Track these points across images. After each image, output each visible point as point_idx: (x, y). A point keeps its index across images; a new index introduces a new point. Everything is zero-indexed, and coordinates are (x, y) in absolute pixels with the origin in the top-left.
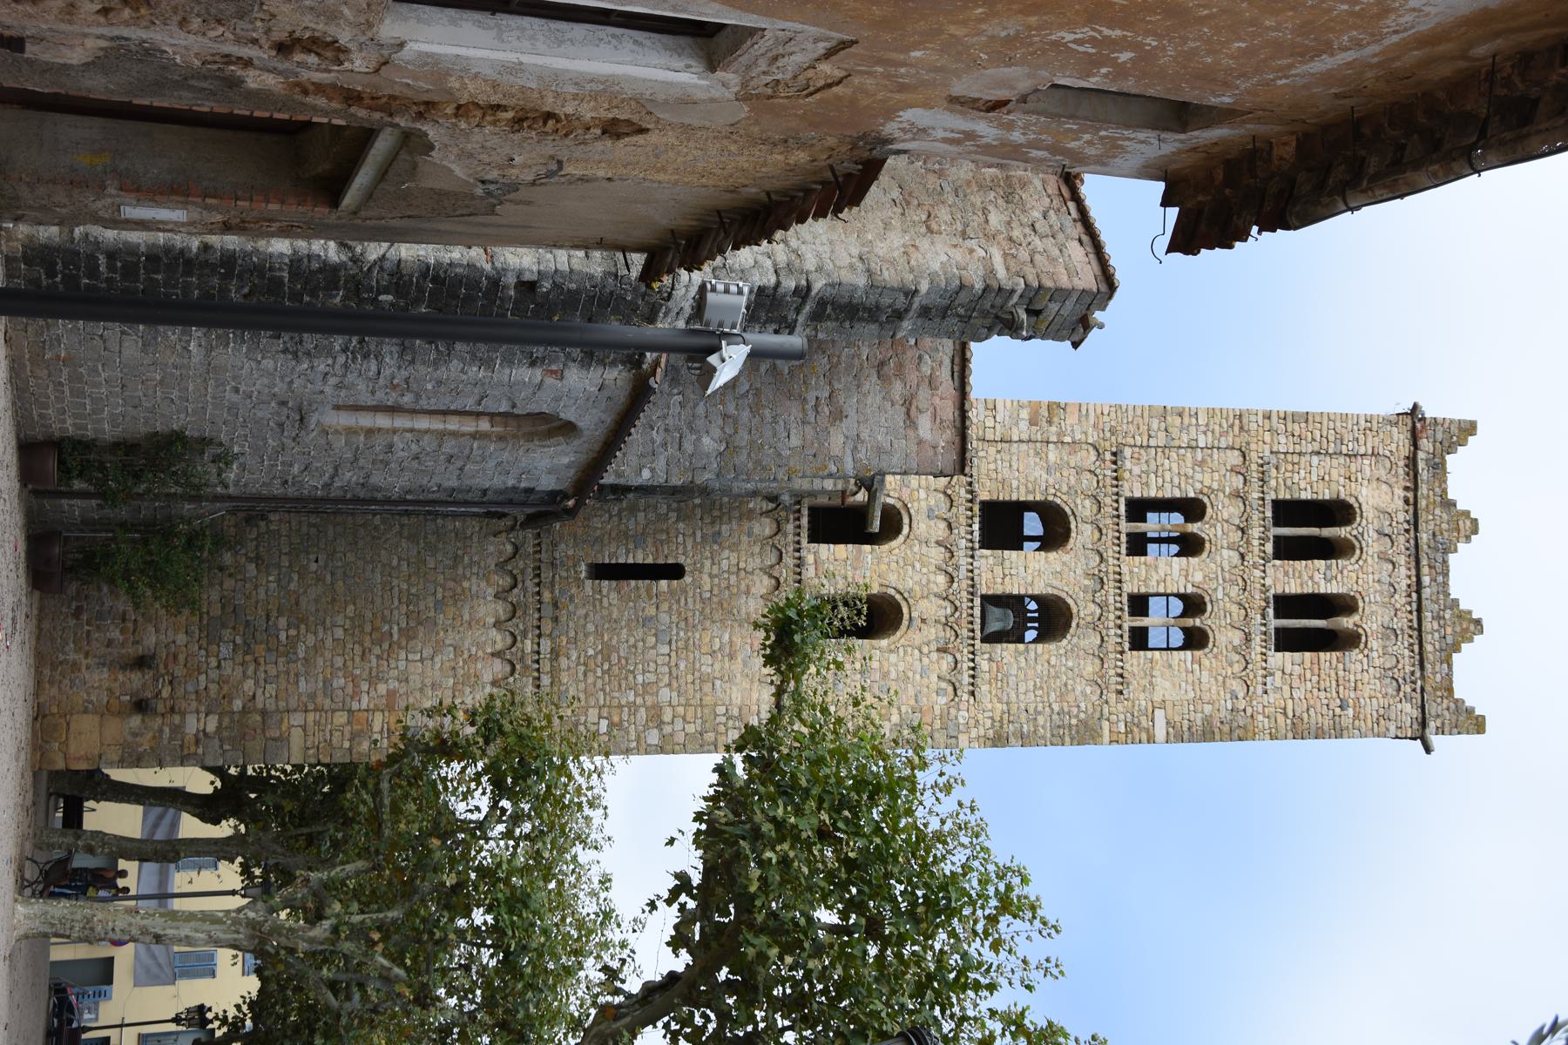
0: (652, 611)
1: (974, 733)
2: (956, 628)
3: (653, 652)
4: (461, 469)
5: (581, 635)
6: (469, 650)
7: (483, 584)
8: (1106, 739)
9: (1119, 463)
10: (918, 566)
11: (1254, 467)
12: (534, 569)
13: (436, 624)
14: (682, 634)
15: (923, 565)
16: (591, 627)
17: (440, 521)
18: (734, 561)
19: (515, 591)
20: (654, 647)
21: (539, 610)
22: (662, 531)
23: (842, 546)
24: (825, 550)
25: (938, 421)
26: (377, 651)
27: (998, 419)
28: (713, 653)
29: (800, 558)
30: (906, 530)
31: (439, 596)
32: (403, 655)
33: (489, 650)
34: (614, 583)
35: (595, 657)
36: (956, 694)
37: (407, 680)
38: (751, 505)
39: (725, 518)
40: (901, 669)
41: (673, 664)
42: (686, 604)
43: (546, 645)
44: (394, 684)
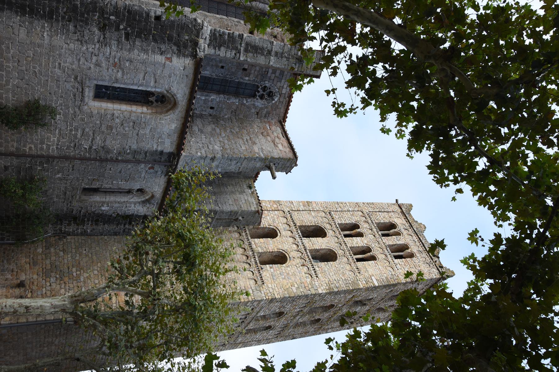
11: (366, 215)
24: (256, 240)
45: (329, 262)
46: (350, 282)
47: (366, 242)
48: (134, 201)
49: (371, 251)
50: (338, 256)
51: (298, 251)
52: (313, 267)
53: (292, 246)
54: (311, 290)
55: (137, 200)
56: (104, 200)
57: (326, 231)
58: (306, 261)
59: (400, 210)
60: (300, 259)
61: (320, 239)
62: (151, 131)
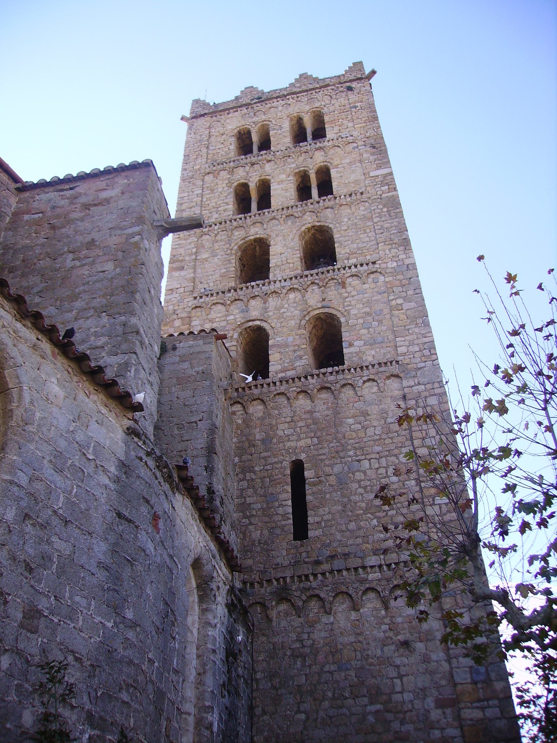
0: (333, 480)
1: (402, 256)
2: (327, 280)
3: (369, 472)
4: (66, 522)
5: (361, 533)
6: (385, 632)
7: (319, 627)
8: (394, 193)
9: (210, 224)
10: (283, 310)
11: (214, 168)
12: (301, 581)
13: (362, 668)
14: (351, 453)
15: (283, 307)
16: (352, 526)
17: (259, 676)
18: (286, 425)
19: (322, 595)
20: (365, 473)
21: (339, 571)
22: (263, 482)
23: (271, 358)
24: (273, 368)
25: (107, 187)
26: (396, 725)
27: (180, 286)
28: (365, 428)
29: (281, 381)
30: (258, 323)
31: (333, 668)
32: (397, 697)
33: (383, 612)
34: (310, 513)
35: (379, 518)
36: (376, 272)
37: (423, 689)
38: (240, 422)
39: (251, 438)
40: (362, 305)
41: (377, 456)
42: (324, 454)
43: (373, 560)
44: (430, 702)
45: (335, 240)
48: (197, 626)
55: (196, 618)
56: (191, 720)
57: (252, 238)
59: (208, 118)
62: (59, 471)
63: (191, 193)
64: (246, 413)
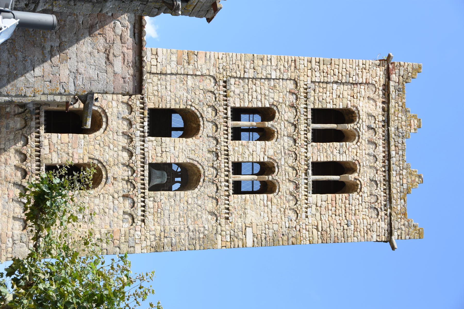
29: (39, 142)
38: (8, 110)
46: (201, 236)
47: (271, 152)
49: (274, 172)
50: (202, 180)
51: (128, 166)
52: (144, 202)
53: (120, 153)
54: (122, 246)
57: (201, 123)
58: (134, 188)
60: (125, 182)
61: (322, 158)
63: (274, 67)
64: (15, 115)
